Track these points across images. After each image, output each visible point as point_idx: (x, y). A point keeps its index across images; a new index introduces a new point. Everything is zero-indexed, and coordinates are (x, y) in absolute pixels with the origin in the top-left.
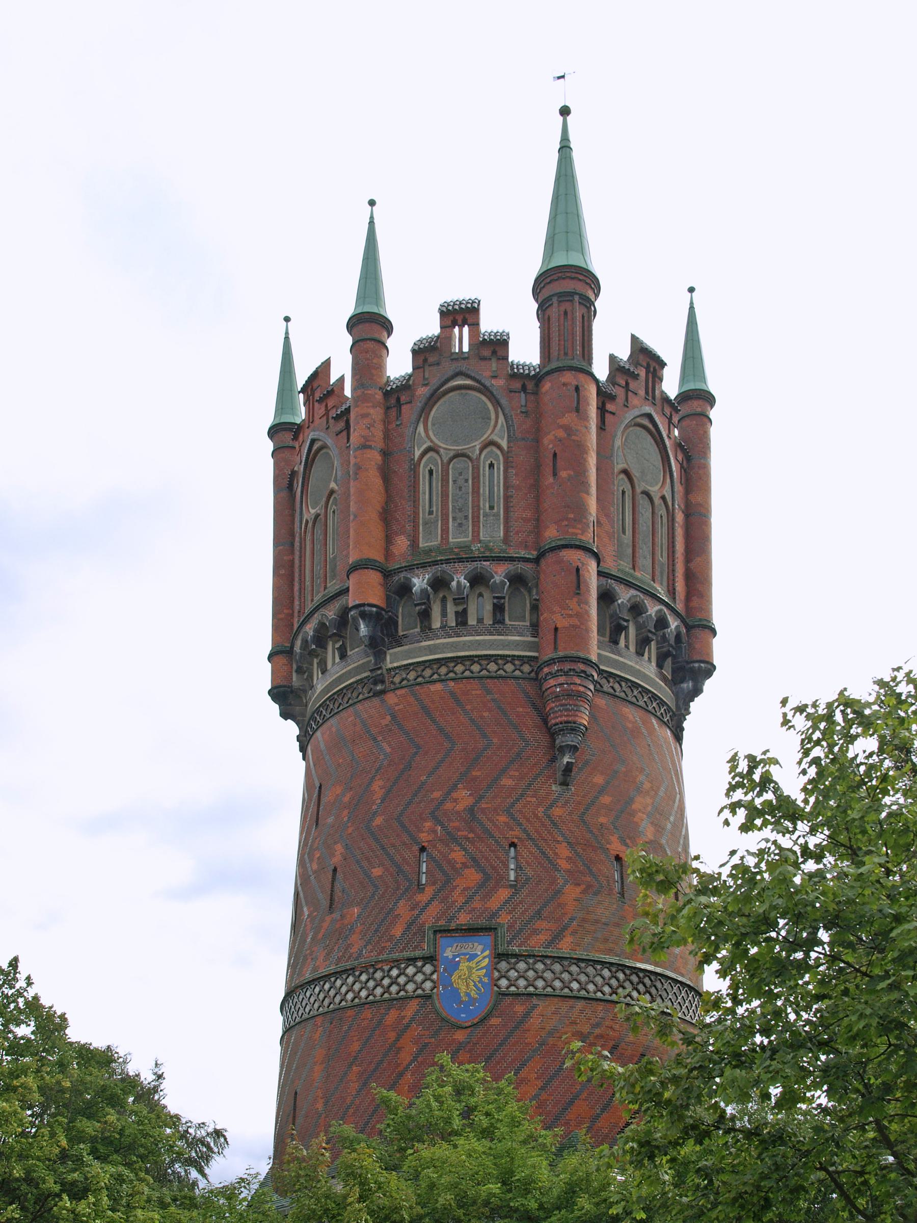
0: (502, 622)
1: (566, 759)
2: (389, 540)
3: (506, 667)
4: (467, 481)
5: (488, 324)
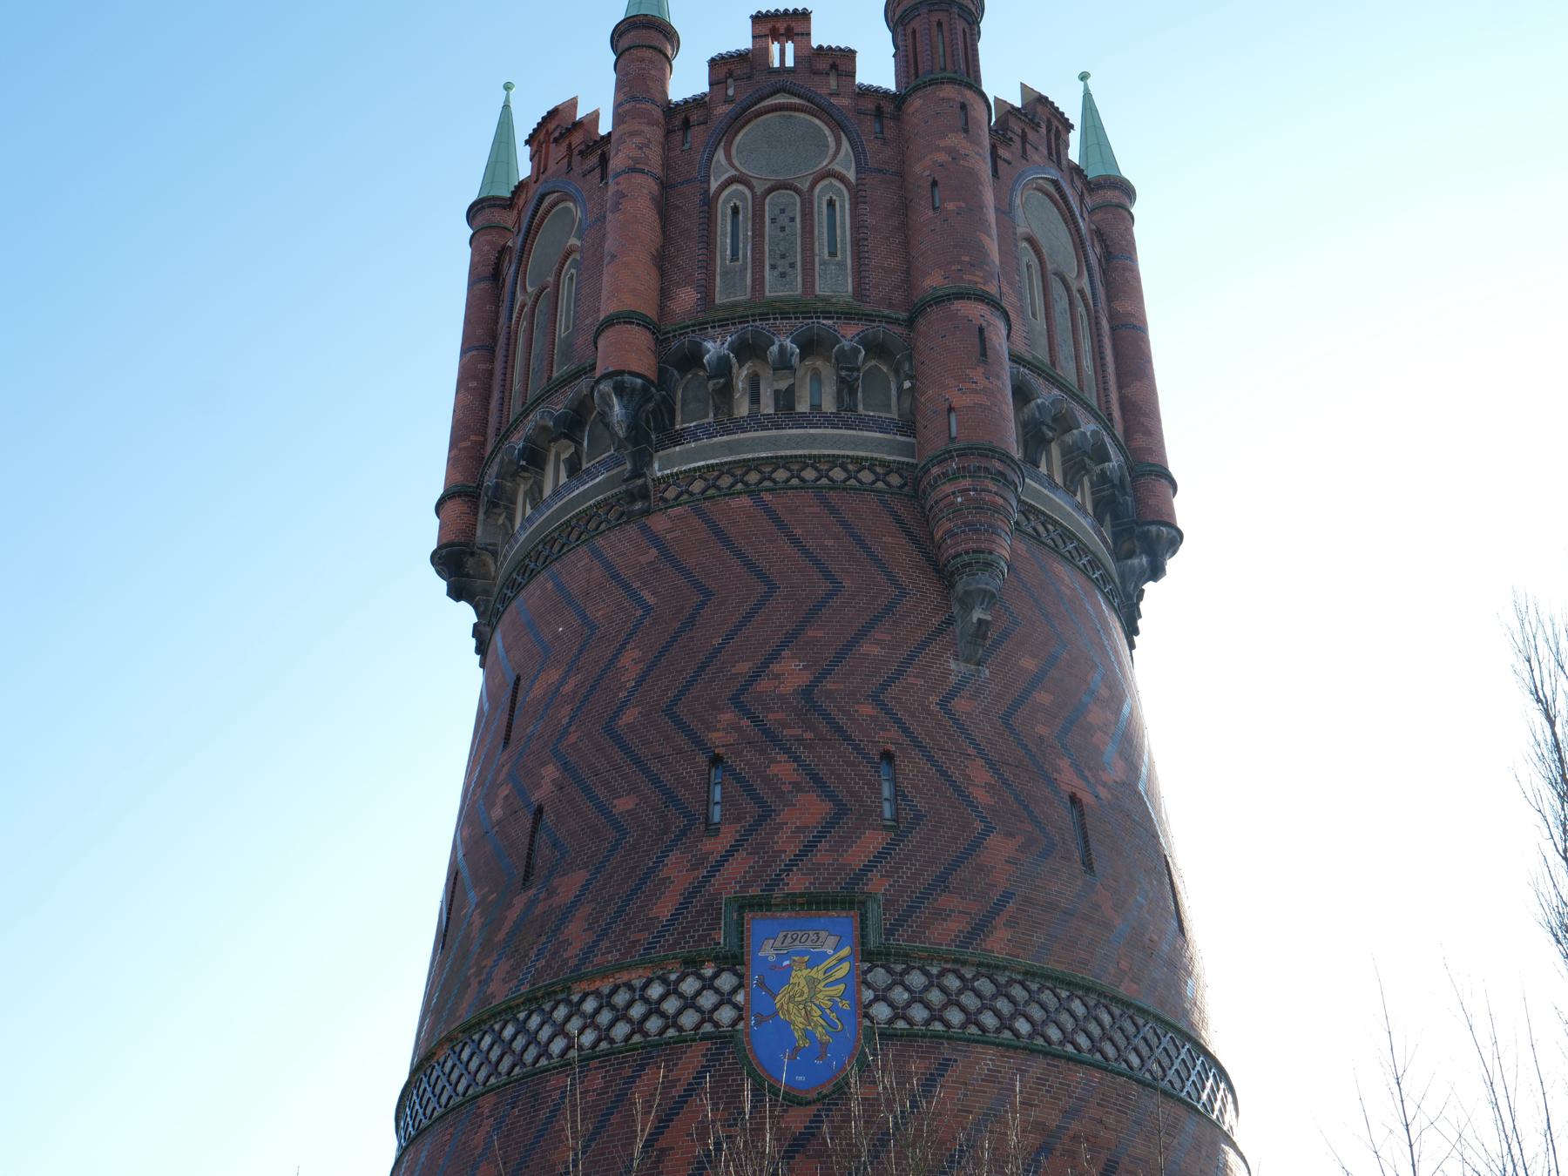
0: (854, 409)
1: (977, 614)
2: (665, 294)
3: (861, 475)
4: (792, 220)
5: (822, 35)
